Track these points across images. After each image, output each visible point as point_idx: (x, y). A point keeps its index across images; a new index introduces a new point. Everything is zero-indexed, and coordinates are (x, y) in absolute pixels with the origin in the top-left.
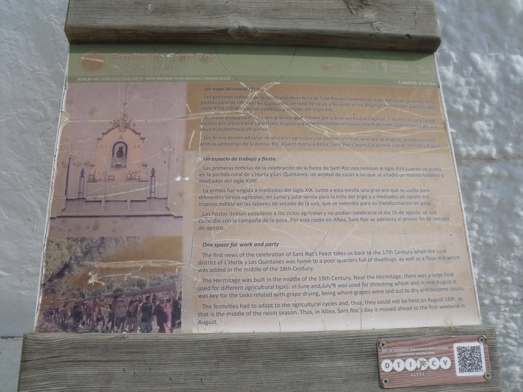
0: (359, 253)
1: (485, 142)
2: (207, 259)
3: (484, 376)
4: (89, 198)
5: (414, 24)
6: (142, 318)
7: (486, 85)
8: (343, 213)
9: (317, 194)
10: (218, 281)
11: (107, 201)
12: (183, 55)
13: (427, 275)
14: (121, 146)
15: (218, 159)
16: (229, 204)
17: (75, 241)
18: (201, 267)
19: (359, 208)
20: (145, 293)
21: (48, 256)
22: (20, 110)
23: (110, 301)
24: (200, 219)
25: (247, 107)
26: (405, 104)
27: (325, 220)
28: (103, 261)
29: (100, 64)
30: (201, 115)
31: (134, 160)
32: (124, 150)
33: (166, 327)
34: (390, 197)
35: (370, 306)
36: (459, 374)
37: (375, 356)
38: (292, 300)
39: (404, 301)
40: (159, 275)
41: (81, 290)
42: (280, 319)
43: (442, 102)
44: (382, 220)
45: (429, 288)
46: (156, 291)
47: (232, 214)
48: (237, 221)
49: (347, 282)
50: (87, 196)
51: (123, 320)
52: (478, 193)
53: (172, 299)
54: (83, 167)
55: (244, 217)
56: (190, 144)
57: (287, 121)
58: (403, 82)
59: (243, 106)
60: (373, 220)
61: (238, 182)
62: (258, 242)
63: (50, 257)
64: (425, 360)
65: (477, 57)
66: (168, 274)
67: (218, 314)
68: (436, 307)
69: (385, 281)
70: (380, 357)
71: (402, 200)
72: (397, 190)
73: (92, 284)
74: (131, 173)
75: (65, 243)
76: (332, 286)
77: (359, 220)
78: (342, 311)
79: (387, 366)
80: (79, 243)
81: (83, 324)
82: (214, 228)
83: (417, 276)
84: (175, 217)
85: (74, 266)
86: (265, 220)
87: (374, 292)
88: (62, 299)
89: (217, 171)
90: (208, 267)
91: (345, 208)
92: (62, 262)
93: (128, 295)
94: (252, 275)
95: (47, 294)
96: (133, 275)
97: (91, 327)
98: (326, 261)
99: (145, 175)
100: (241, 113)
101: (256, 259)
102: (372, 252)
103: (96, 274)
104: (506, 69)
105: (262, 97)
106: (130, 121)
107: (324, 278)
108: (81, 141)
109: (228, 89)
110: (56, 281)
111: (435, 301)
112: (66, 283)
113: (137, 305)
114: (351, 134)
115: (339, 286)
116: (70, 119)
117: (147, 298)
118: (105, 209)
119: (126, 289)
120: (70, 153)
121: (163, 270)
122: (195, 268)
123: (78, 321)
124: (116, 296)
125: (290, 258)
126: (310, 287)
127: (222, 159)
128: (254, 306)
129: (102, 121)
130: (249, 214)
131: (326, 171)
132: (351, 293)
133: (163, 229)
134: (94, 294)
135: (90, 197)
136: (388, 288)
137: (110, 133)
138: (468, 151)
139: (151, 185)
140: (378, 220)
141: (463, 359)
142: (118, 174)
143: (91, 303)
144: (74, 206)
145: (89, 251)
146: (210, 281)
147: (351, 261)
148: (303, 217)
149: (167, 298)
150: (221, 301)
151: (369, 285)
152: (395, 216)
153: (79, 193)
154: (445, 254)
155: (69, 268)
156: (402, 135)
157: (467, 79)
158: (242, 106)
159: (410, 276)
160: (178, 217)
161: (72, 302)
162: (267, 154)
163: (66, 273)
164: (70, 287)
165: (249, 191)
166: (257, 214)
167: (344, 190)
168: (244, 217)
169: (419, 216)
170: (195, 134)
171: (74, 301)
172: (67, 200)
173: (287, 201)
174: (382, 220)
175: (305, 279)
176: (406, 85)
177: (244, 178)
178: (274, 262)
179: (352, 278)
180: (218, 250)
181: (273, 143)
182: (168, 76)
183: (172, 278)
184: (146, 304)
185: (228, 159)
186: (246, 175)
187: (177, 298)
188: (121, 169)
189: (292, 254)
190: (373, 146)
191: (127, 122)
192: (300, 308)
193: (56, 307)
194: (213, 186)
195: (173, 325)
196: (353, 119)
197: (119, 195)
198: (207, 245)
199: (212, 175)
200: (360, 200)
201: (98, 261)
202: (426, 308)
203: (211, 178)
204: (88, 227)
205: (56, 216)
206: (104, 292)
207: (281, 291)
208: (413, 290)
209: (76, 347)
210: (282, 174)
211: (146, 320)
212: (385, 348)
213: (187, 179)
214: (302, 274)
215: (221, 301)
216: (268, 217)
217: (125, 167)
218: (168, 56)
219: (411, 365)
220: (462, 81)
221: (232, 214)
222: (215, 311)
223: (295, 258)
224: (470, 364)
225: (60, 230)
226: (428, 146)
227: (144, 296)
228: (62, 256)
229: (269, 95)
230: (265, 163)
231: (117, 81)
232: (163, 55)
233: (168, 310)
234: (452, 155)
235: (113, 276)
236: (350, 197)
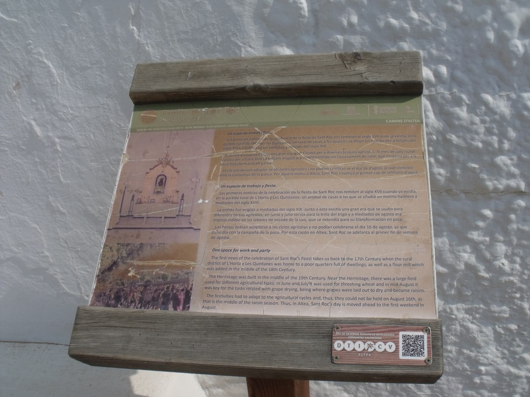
1: (511, 176)
2: (214, 261)
3: (425, 361)
4: (136, 215)
5: (398, 72)
7: (501, 122)
8: (325, 227)
9: (306, 213)
10: (220, 277)
11: (147, 218)
12: (214, 109)
13: (392, 278)
16: (236, 220)
18: (210, 266)
19: (339, 223)
20: (167, 284)
21: (103, 256)
22: (111, 158)
23: (141, 289)
26: (390, 139)
28: (140, 260)
29: (154, 119)
31: (170, 188)
32: (164, 181)
34: (366, 215)
35: (338, 302)
36: (401, 357)
37: (330, 338)
38: (275, 294)
39: (369, 299)
41: (123, 281)
43: (423, 135)
46: (175, 283)
49: (322, 281)
51: (149, 303)
52: (515, 226)
54: (134, 193)
55: (246, 230)
57: (289, 156)
58: (390, 121)
59: (255, 146)
60: (350, 233)
62: (254, 249)
63: (104, 256)
64: (372, 343)
65: (488, 98)
66: (185, 271)
67: (218, 302)
68: (397, 305)
69: (354, 281)
70: (333, 338)
71: (377, 217)
72: (373, 209)
75: (115, 247)
77: (338, 233)
78: (315, 304)
79: (338, 345)
81: (121, 304)
82: (222, 238)
83: (383, 279)
84: (195, 229)
86: (262, 232)
88: (109, 286)
89: (229, 196)
90: (215, 266)
91: (327, 223)
93: (154, 285)
94: (247, 273)
101: (251, 261)
102: (346, 258)
104: (517, 105)
105: (271, 138)
107: (303, 278)
108: (134, 175)
109: (246, 133)
111: (396, 300)
114: (339, 165)
116: (129, 159)
117: (168, 288)
120: (126, 183)
121: (181, 268)
123: (118, 302)
128: (246, 297)
130: (250, 228)
131: (315, 195)
132: (324, 290)
133: (185, 238)
136: (356, 287)
137: (156, 168)
138: (494, 185)
140: (354, 233)
141: (407, 345)
142: (158, 198)
143: (129, 289)
144: (127, 221)
145: (132, 253)
148: (292, 230)
150: (221, 292)
151: (340, 284)
152: (369, 230)
153: (129, 212)
154: (410, 262)
156: (384, 164)
157: (481, 118)
159: (376, 279)
160: (197, 229)
162: (269, 182)
164: (115, 278)
165: (252, 210)
166: (257, 227)
168: (246, 230)
172: (121, 216)
173: (280, 217)
174: (357, 232)
175: (287, 278)
176: (393, 123)
177: (249, 200)
179: (327, 278)
180: (223, 254)
182: (202, 125)
183: (187, 273)
184: (166, 292)
185: (239, 186)
186: (252, 198)
189: (279, 259)
192: (281, 300)
194: (225, 206)
198: (215, 250)
200: (341, 217)
202: (388, 305)
203: (225, 201)
204: (132, 236)
207: (268, 286)
208: (378, 290)
209: (110, 316)
212: (338, 331)
214: (286, 274)
215: (221, 292)
216: (264, 230)
217: (163, 193)
218: (203, 110)
219: (360, 346)
220: (477, 120)
221: (237, 227)
222: (216, 299)
223: (282, 262)
224: (413, 350)
225: (113, 238)
226: (406, 173)
227: (166, 286)
228: (113, 256)
230: (267, 189)
231: (165, 130)
232: (199, 110)
233: (182, 297)
234: (427, 179)
236: (332, 214)
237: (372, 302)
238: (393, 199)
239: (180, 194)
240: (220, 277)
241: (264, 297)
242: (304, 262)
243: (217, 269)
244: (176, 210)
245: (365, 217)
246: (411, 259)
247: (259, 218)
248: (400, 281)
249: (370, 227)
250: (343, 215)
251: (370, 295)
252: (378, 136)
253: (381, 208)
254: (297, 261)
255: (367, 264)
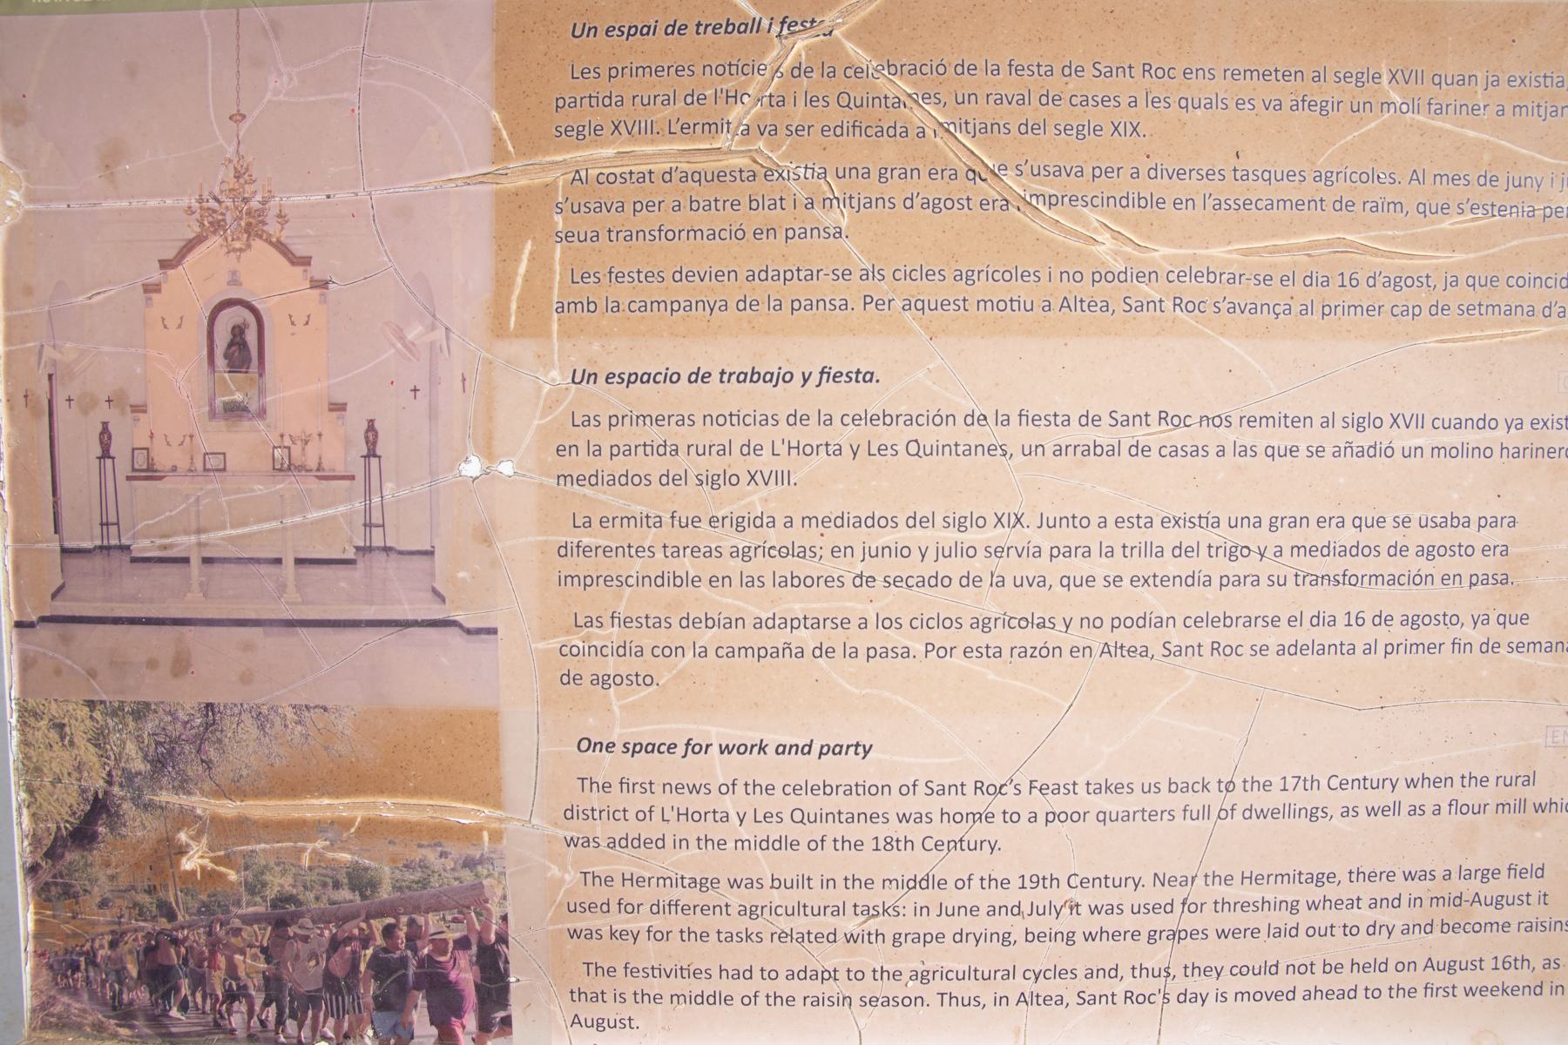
0: (1187, 788)
2: (595, 800)
4: (143, 547)
6: (375, 998)
8: (1143, 621)
10: (637, 881)
11: (207, 561)
13: (1439, 874)
14: (239, 321)
15: (632, 379)
16: (678, 580)
17: (114, 714)
18: (578, 828)
19: (1212, 600)
21: (32, 770)
24: (563, 639)
25: (760, 116)
27: (1066, 652)
28: (220, 792)
30: (556, 166)
31: (294, 378)
32: (251, 337)
33: (459, 1031)
34: (1344, 552)
35: (1197, 984)
38: (910, 958)
39: (1332, 968)
40: (423, 851)
42: (862, 1023)
44: (1297, 649)
45: (1437, 923)
46: (417, 909)
47: (688, 622)
48: (711, 653)
49: (1127, 896)
50: (134, 537)
51: (313, 1000)
53: (474, 940)
55: (735, 637)
56: (514, 306)
57: (937, 189)
60: (1264, 649)
61: (714, 482)
62: (788, 741)
63: (38, 770)
66: (457, 850)
67: (641, 996)
68: (1450, 992)
69: (1272, 892)
73: (193, 872)
74: (287, 442)
75: (81, 723)
76: (1066, 911)
78: (1094, 1000)
80: (132, 725)
81: (184, 1007)
83: (1399, 877)
84: (468, 632)
85: (125, 806)
86: (823, 651)
87: (1222, 934)
90: (601, 830)
91: (1152, 600)
92: (84, 791)
94: (763, 864)
95: (48, 900)
96: (332, 847)
97: (210, 1018)
98: (1052, 817)
99: (337, 447)
100: (730, 152)
102: (1238, 781)
103: (204, 840)
105: (826, 65)
106: (264, 203)
107: (1039, 881)
109: (676, 29)
110: (72, 856)
111: (1450, 967)
112: (108, 865)
113: (354, 952)
114: (1215, 252)
115: (1095, 910)
116: (30, 197)
117: (389, 931)
118: (205, 595)
119: (311, 896)
120: (49, 352)
121: (439, 834)
122: (551, 830)
123: (166, 996)
124: (282, 916)
125: (912, 805)
126: (983, 911)
127: (647, 378)
128: (771, 975)
129: (153, 203)
130: (759, 624)
131: (1089, 435)
132: (1135, 935)
133: (426, 678)
134: (206, 910)
135: (146, 543)
136: (1282, 918)
137: (191, 259)
139: (368, 493)
140: (1282, 650)
142: (239, 443)
143: (198, 938)
145: (170, 752)
146: (608, 881)
147: (1153, 815)
148: (977, 638)
149: (457, 935)
150: (649, 953)
151: (1209, 907)
155: (109, 815)
158: (734, 113)
159: (1370, 877)
160: (479, 631)
161: (136, 931)
163: (101, 829)
164: (123, 882)
165: (759, 522)
166: (791, 623)
167: (1157, 522)
168: (735, 637)
169: (1455, 632)
170: (532, 258)
171: (142, 929)
172: (65, 551)
173: (913, 567)
174: (1297, 649)
175: (964, 883)
177: (738, 464)
178: (851, 819)
179: (1148, 879)
181: (867, 300)
183: (470, 864)
184: (385, 950)
185: (673, 378)
187: (493, 937)
188: (246, 424)
189: (921, 788)
190: (1305, 311)
191: (254, 204)
192: (938, 985)
193: (88, 946)
194: (612, 500)
195: (485, 1027)
196: (1229, 175)
197: (250, 535)
198: (593, 745)
199: (606, 451)
201: (203, 793)
203: (605, 464)
204: (152, 664)
205: (34, 618)
206: (238, 903)
207: (872, 925)
208: (1373, 929)
210: (901, 448)
211: (391, 1003)
213: (506, 468)
214: (955, 865)
221: (688, 622)
222: (629, 986)
227: (378, 925)
228: (79, 769)
229: (857, 53)
230: (834, 397)
233: (465, 974)
235: (264, 850)
236: (1180, 551)
237: (1346, 980)
238: (1477, 462)
239: (355, 424)
240: (637, 881)
241: (856, 975)
242: (1040, 804)
243: (612, 844)
244: (348, 517)
245: (1334, 566)
246: (1529, 781)
247: (804, 567)
248: (1474, 885)
249: (1360, 621)
250: (1232, 555)
251: (1338, 949)
252: (1419, 78)
253: (1415, 516)
254: (1008, 802)
255: (1334, 810)
